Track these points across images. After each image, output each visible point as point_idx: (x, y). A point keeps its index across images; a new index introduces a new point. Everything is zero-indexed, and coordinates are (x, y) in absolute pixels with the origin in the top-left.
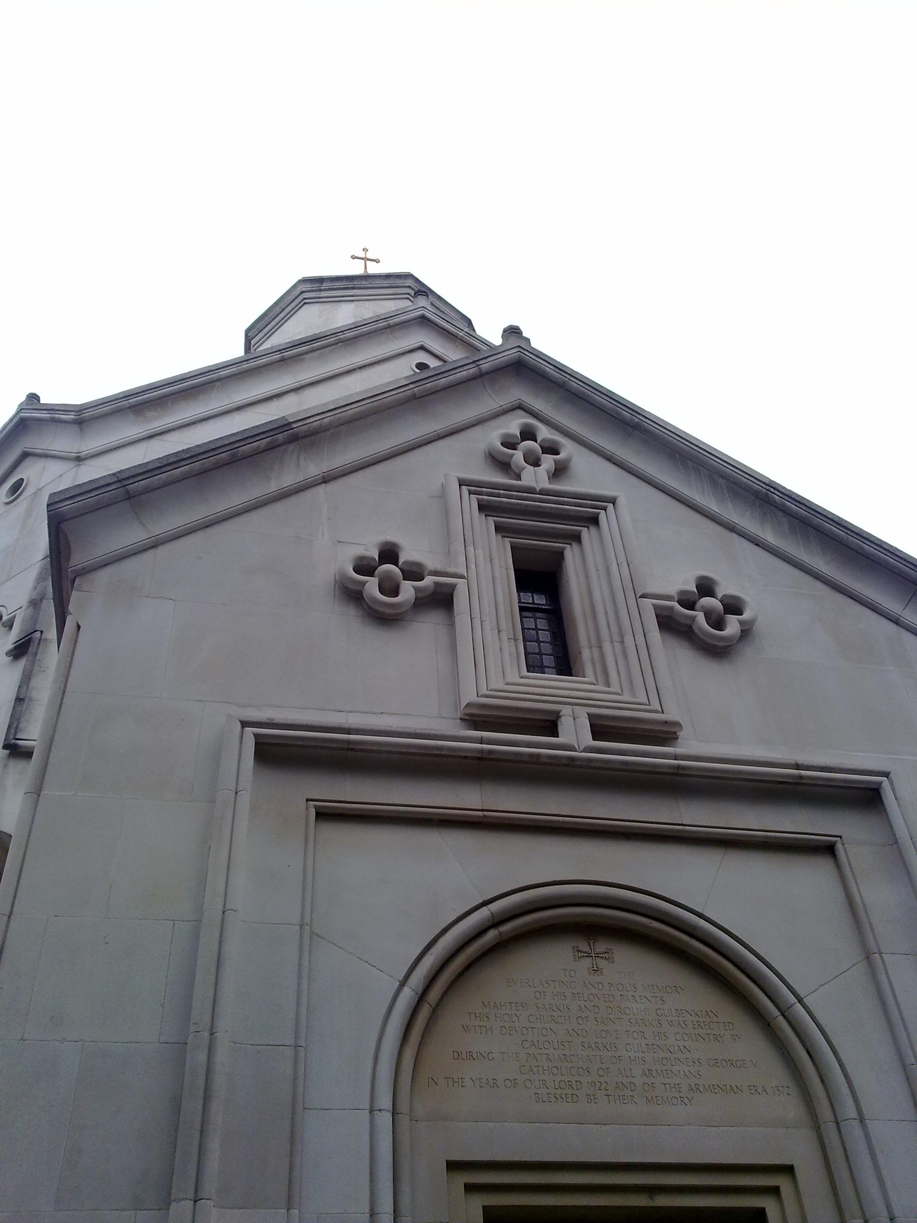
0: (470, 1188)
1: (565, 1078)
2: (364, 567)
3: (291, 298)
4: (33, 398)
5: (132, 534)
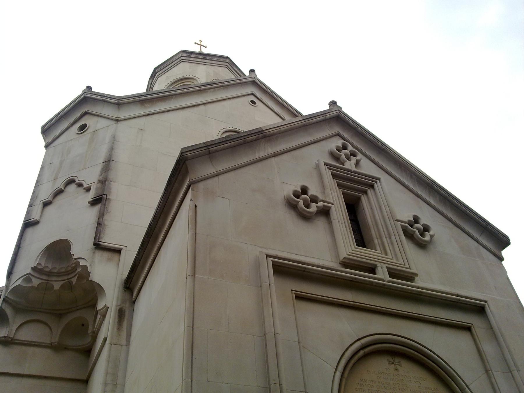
2: (297, 195)
3: (176, 58)
4: (89, 88)
5: (209, 169)
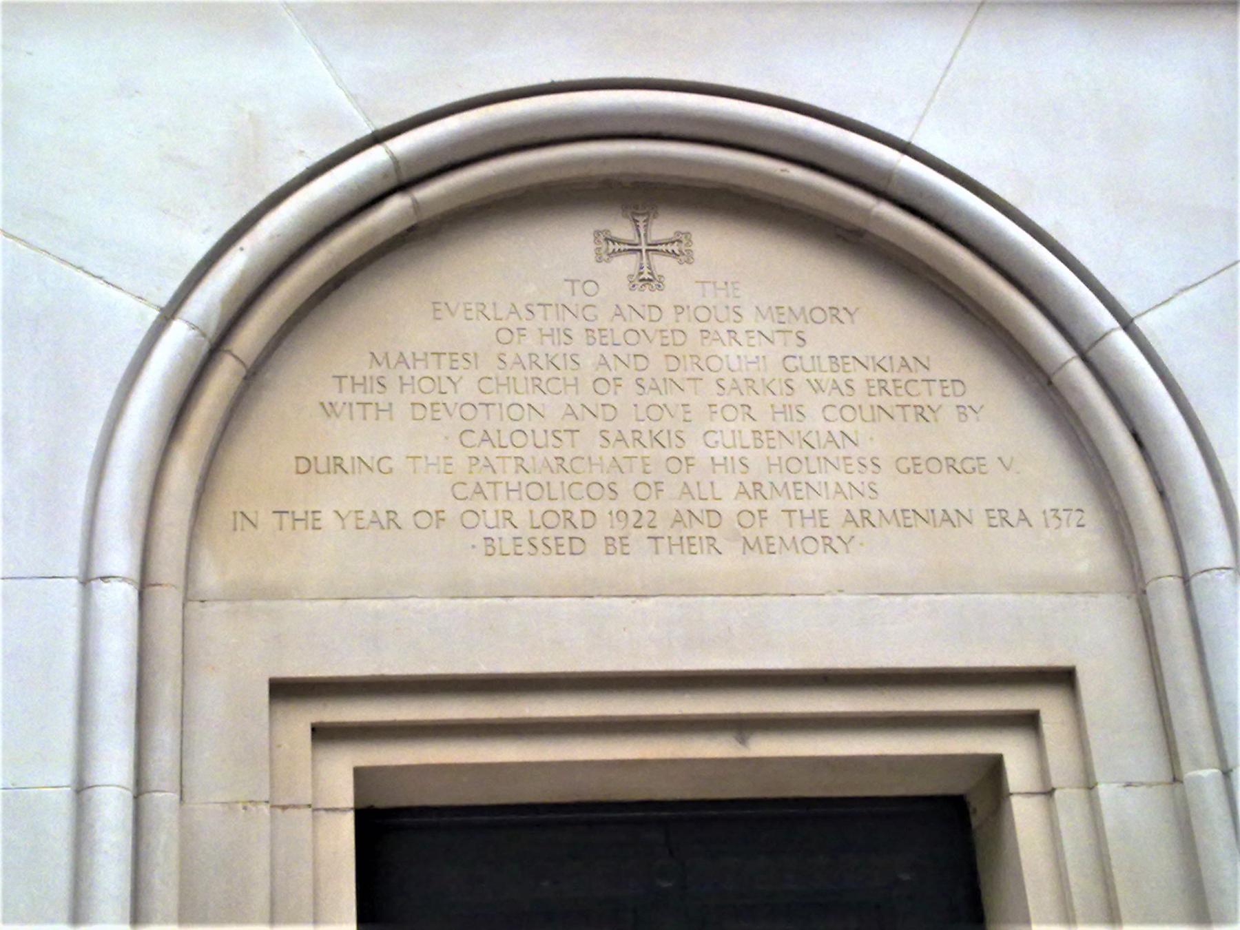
0: (323, 734)
1: (558, 506)
